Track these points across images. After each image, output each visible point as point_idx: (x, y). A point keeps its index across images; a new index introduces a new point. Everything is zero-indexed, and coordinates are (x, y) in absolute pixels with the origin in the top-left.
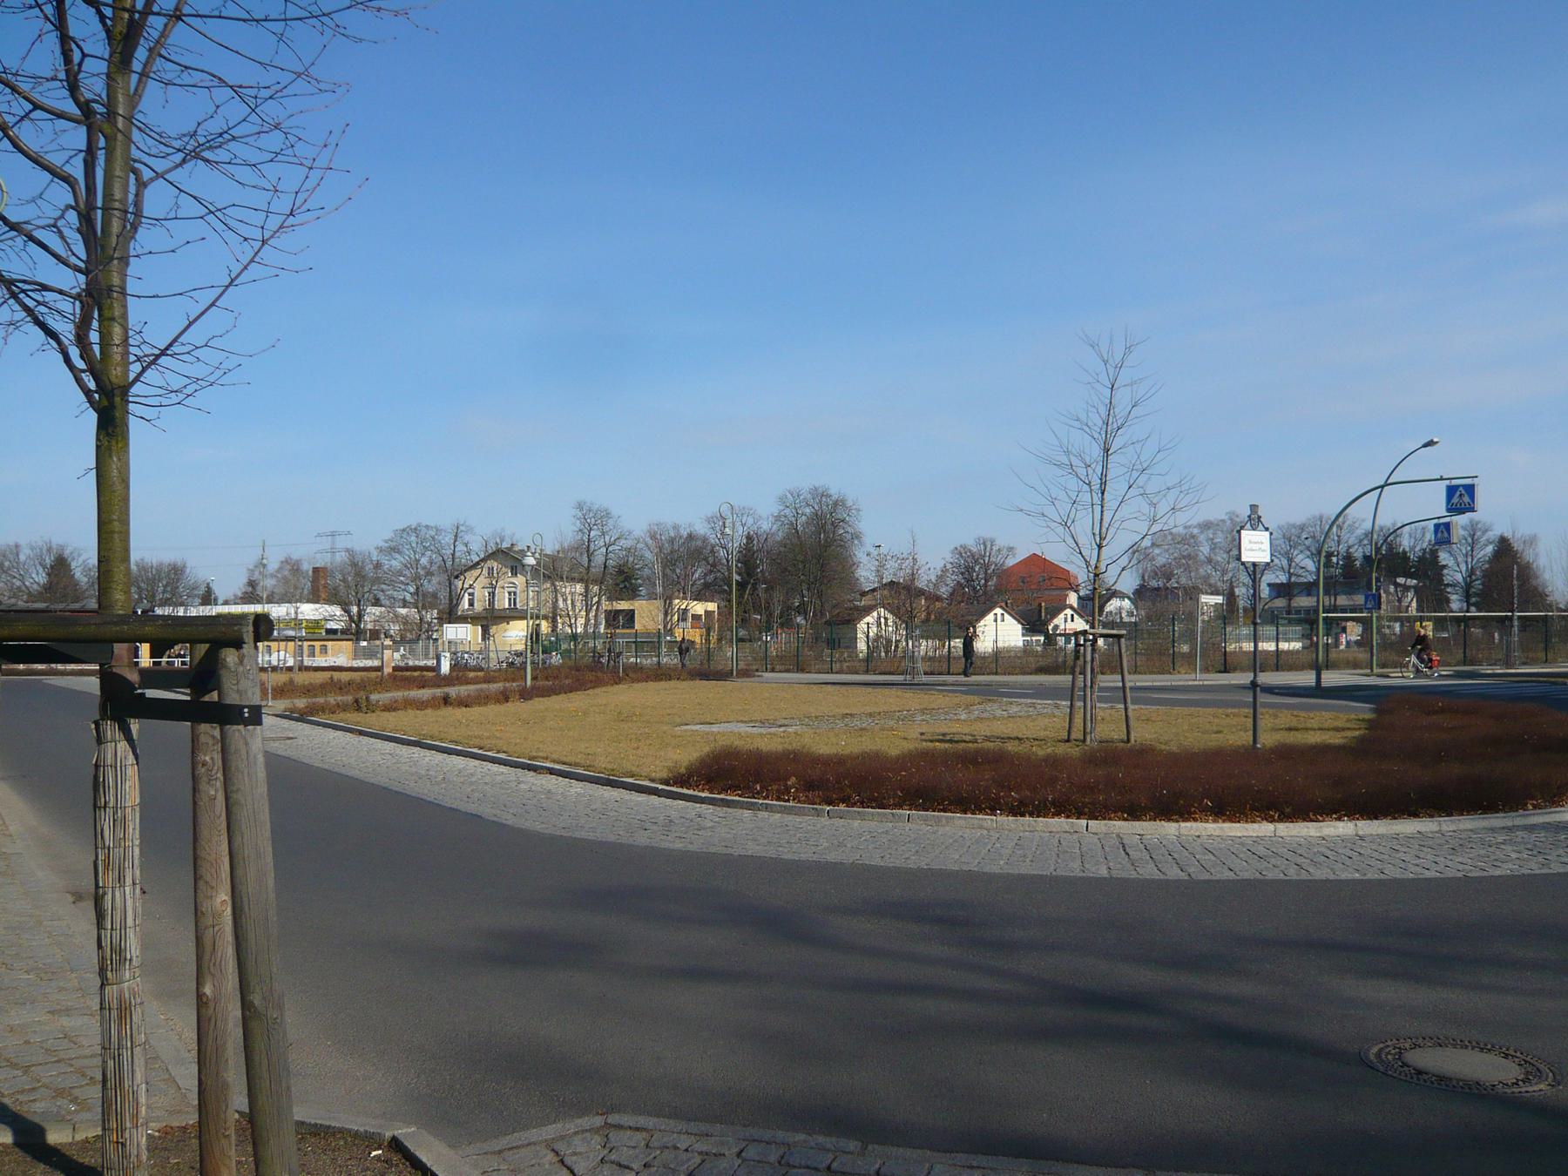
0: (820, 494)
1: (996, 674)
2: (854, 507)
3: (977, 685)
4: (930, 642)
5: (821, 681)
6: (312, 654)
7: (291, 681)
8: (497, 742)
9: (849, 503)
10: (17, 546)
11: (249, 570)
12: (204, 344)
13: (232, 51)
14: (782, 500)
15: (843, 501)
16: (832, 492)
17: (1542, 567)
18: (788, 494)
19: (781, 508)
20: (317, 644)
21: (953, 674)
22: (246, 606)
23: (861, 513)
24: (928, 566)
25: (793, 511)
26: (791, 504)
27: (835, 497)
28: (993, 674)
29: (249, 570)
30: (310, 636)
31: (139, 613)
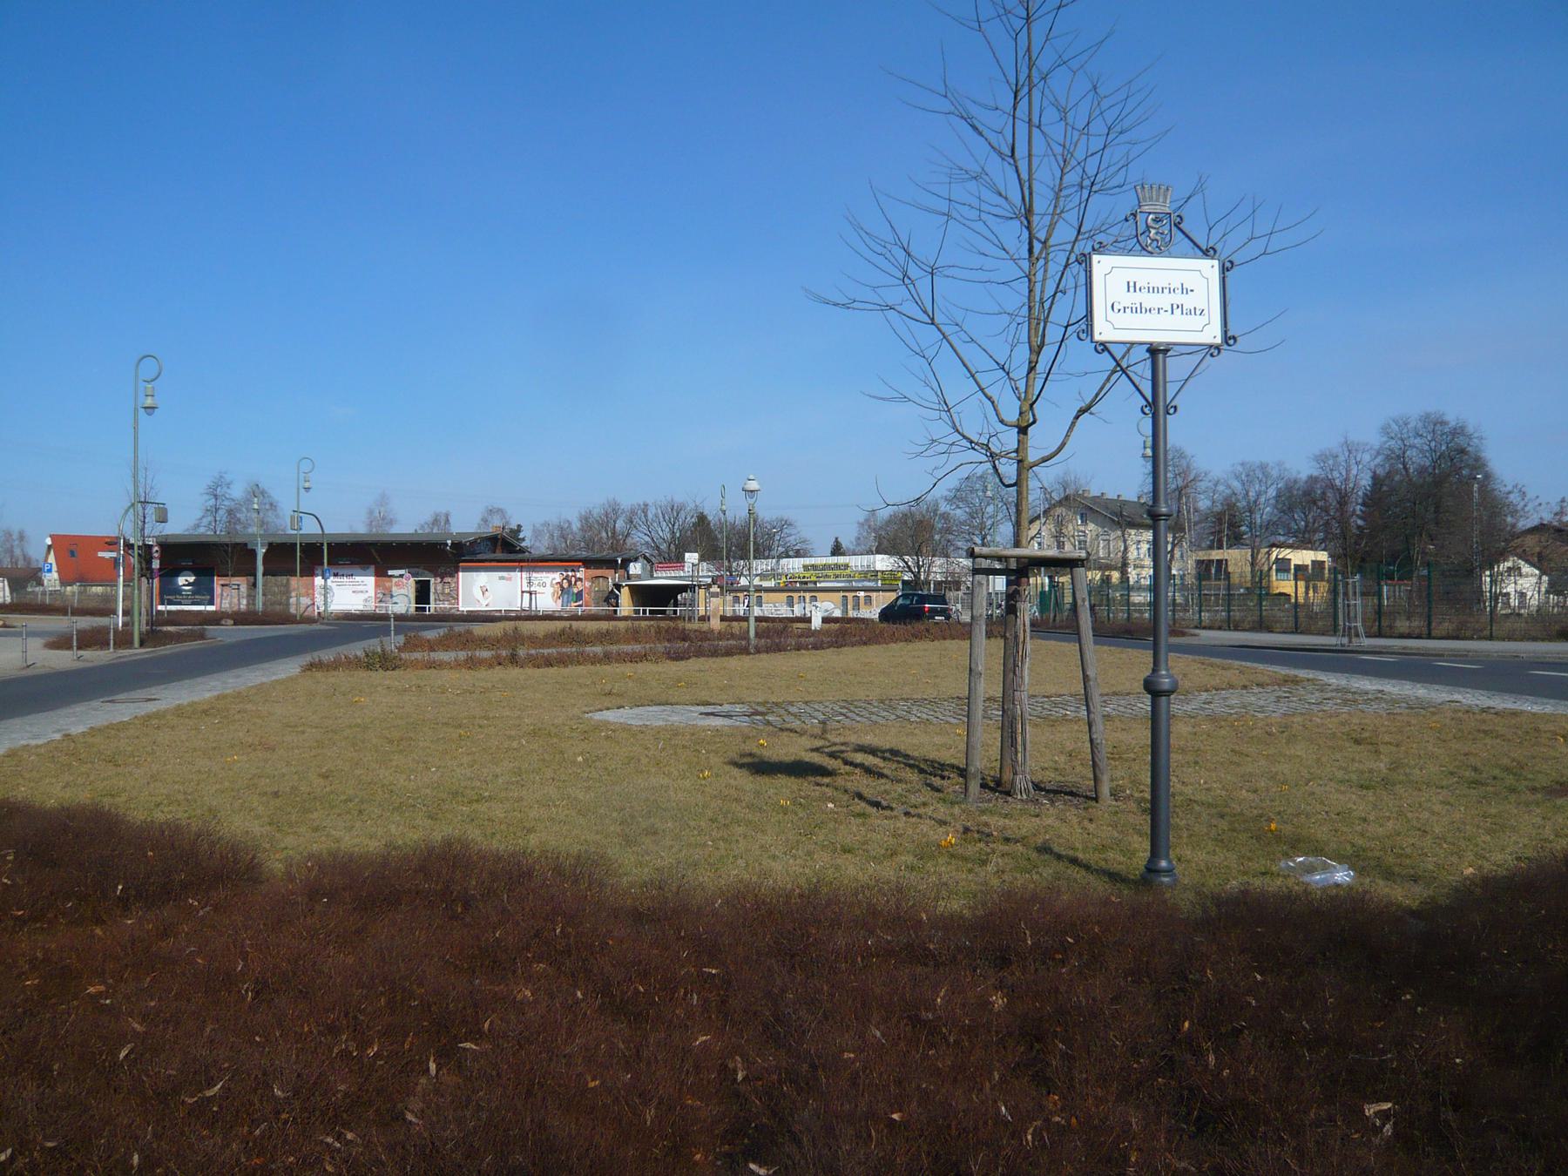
0: (1435, 423)
1: (1491, 638)
2: (1476, 435)
3: (1423, 655)
4: (926, 592)
5: (1237, 644)
6: (857, 606)
7: (469, 632)
8: (1514, 722)
9: (1470, 429)
10: (646, 505)
11: (858, 523)
12: (933, 326)
13: (1040, 117)
14: (1385, 430)
15: (1462, 428)
16: (1447, 418)
17: (598, 518)
18: (1391, 422)
19: (1385, 439)
20: (795, 595)
21: (1434, 638)
22: (836, 558)
23: (1483, 441)
24: (1538, 501)
25: (1399, 442)
26: (1396, 435)
27: (1453, 424)
28: (1375, 636)
29: (858, 523)
30: (887, 587)
31: (620, 562)
